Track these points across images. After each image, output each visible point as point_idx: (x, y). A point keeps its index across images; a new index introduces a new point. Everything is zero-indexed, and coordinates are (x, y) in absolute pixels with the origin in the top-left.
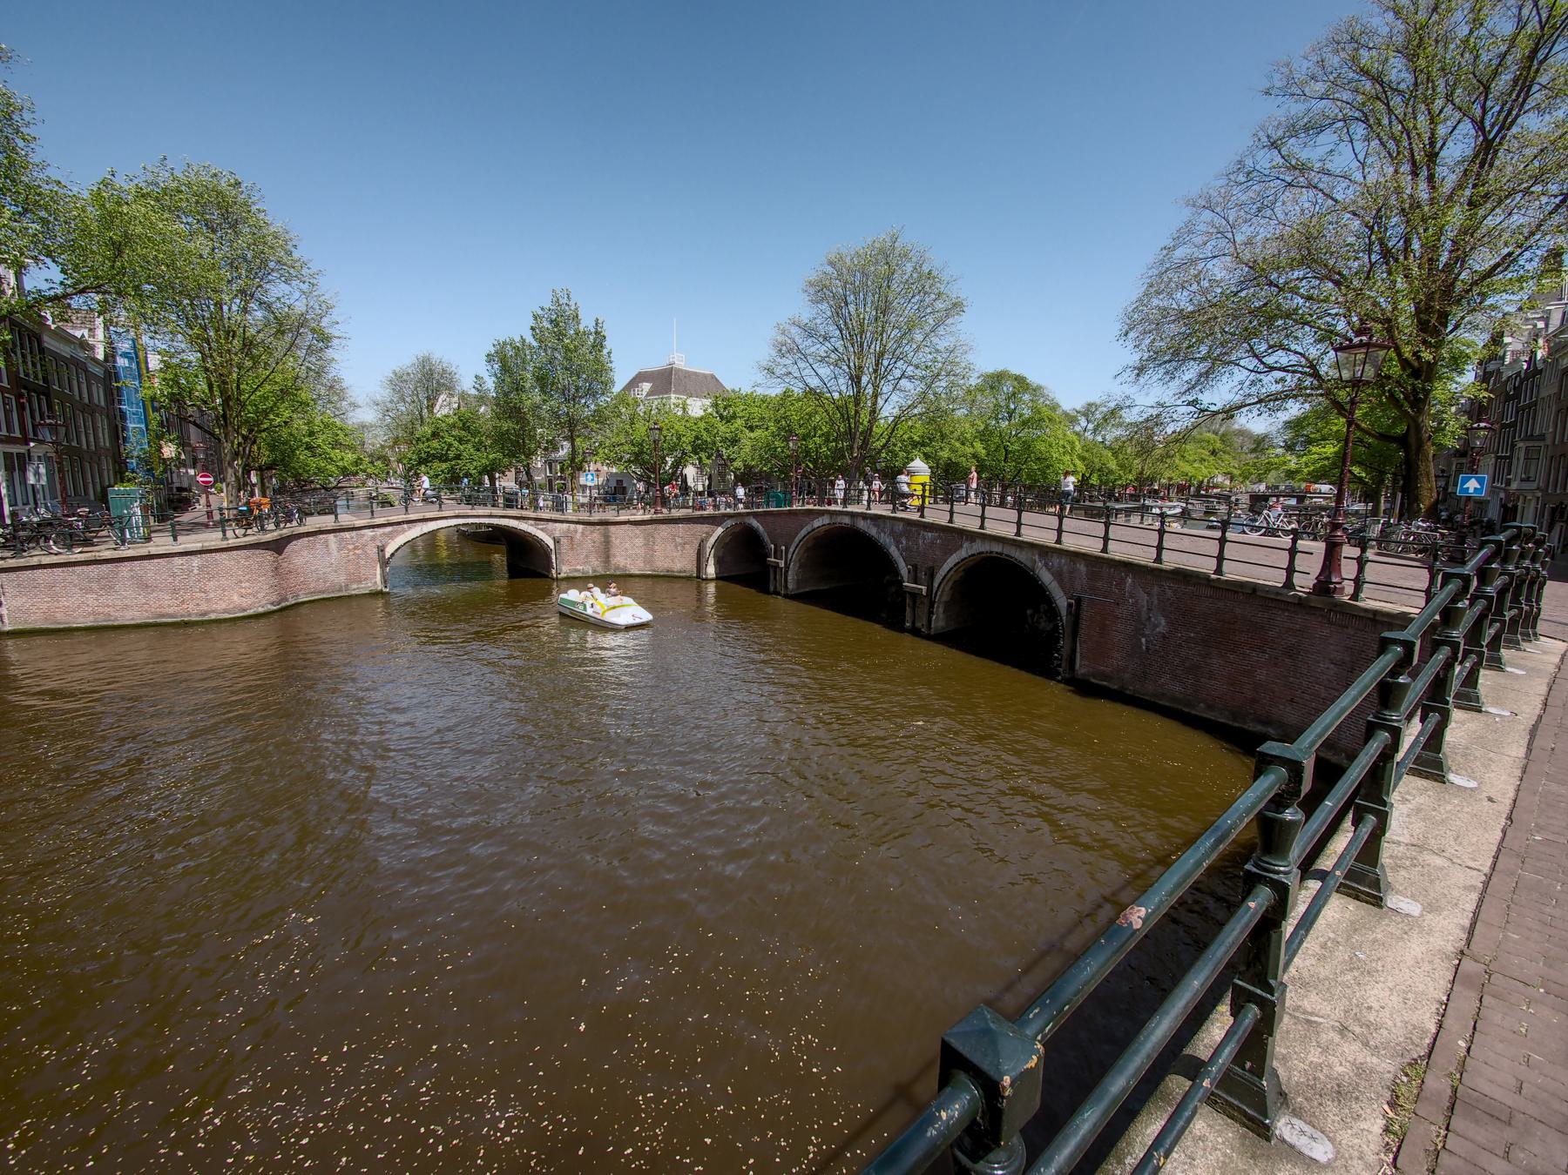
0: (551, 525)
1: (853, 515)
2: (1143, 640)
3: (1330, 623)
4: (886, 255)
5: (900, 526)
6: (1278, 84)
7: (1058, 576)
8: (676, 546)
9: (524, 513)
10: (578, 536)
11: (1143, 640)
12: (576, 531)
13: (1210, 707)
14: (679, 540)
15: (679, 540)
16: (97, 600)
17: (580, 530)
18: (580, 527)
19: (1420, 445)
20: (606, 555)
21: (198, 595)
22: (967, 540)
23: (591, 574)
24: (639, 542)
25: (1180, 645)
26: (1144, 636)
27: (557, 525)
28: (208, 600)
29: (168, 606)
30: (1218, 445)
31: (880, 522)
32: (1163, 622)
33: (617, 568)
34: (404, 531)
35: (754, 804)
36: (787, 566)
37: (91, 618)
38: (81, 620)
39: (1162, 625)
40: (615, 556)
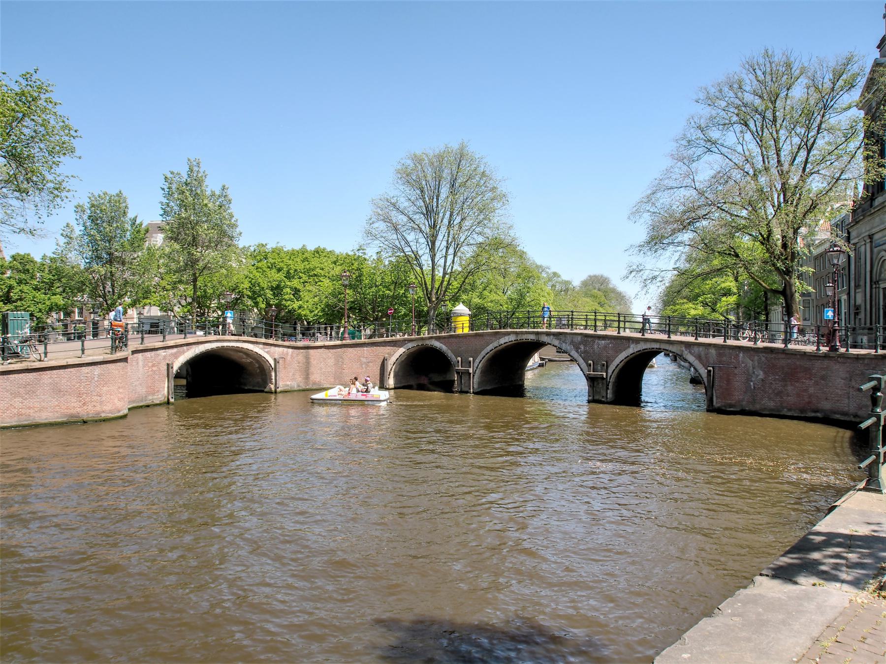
0: (273, 349)
1: (537, 333)
2: (752, 383)
3: (839, 363)
4: (461, 156)
5: (579, 338)
6: (702, 98)
7: (699, 357)
8: (361, 365)
9: (258, 340)
10: (289, 358)
11: (752, 383)
12: (287, 354)
13: (790, 410)
14: (364, 360)
15: (364, 360)
16: (22, 403)
17: (290, 354)
18: (290, 350)
19: (792, 295)
20: (306, 372)
21: (96, 398)
22: (633, 343)
23: (296, 388)
24: (331, 362)
25: (771, 383)
26: (752, 381)
27: (277, 349)
28: (101, 403)
29: (74, 407)
30: (603, 298)
31: (561, 337)
32: (761, 373)
33: (314, 383)
34: (184, 352)
35: (332, 605)
36: (474, 373)
37: (16, 419)
38: (8, 420)
39: (761, 375)
40: (313, 374)
